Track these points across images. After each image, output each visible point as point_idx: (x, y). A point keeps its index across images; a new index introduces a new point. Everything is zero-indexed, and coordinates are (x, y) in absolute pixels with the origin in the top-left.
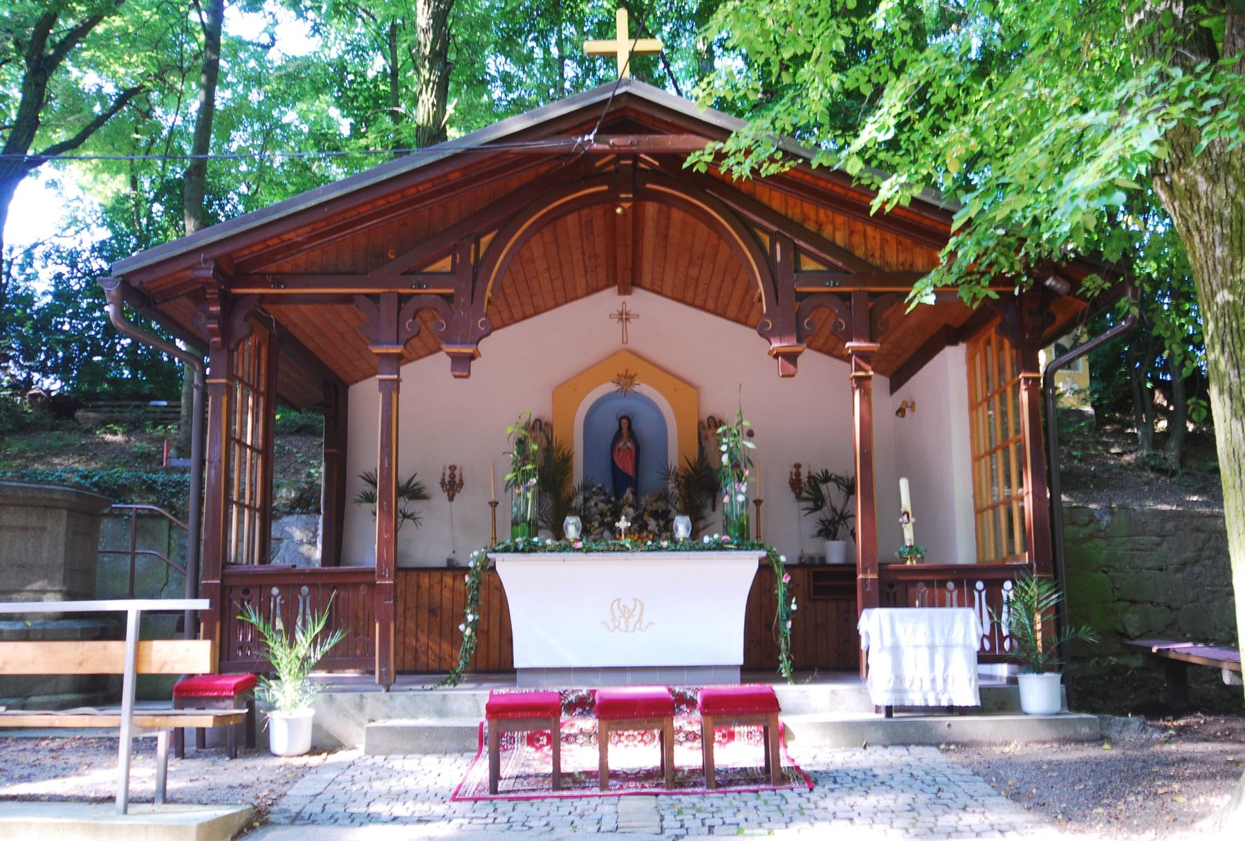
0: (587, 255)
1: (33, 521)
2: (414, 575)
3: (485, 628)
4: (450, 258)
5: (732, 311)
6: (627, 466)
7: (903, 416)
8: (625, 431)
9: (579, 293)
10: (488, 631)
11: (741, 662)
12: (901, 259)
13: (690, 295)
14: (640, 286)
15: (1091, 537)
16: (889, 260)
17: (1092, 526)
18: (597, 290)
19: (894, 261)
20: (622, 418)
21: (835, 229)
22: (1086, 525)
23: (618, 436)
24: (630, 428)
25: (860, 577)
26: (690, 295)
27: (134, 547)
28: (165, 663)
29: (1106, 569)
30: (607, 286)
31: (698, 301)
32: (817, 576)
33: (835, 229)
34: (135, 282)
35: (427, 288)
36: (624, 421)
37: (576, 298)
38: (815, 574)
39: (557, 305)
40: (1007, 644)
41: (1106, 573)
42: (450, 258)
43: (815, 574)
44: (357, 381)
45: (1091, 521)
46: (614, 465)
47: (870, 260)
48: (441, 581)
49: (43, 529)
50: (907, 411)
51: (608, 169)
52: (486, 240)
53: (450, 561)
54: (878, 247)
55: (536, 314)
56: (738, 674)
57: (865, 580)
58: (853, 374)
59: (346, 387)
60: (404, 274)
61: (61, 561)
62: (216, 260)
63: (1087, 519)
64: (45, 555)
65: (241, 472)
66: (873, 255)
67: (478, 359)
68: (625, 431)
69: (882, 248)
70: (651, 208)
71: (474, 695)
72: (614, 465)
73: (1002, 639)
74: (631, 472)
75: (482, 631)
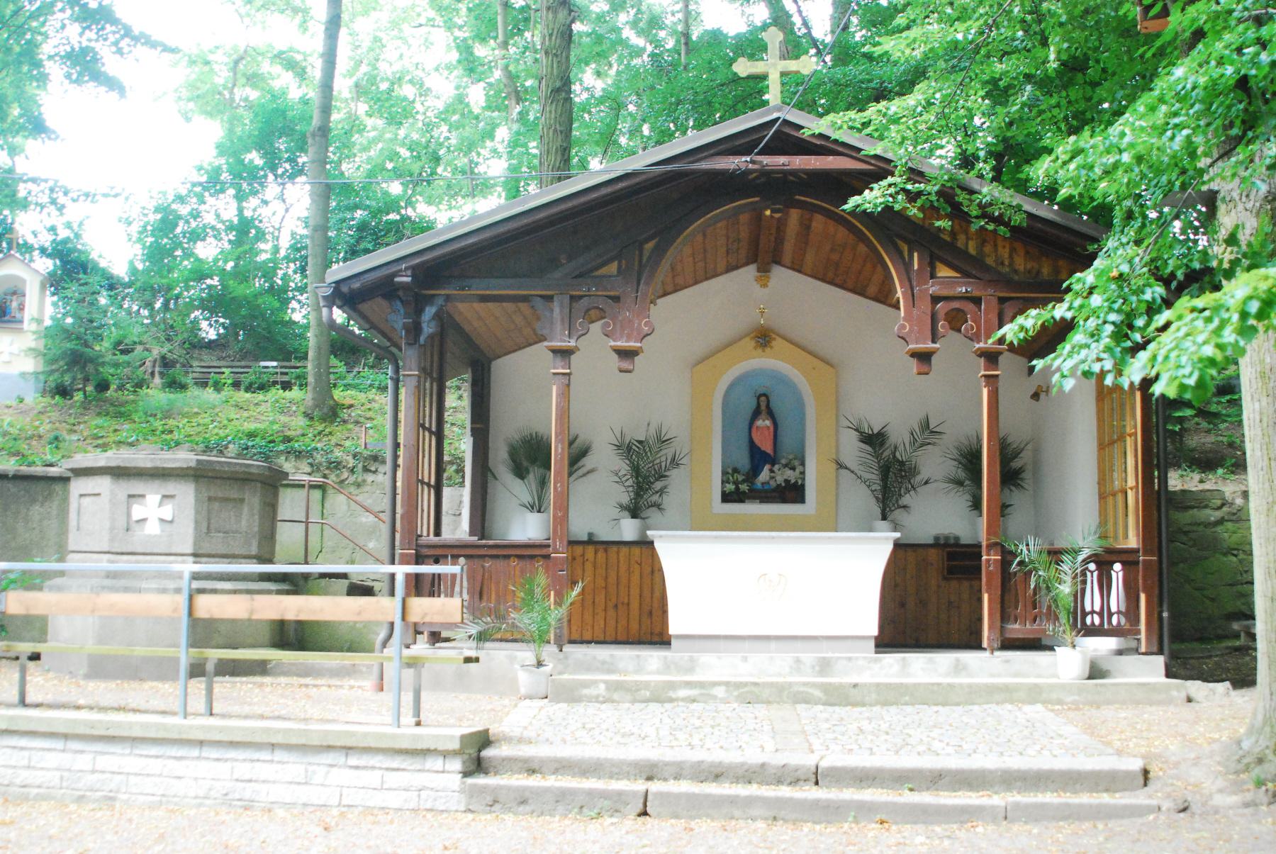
0: (731, 240)
1: (234, 494)
2: (615, 548)
3: (626, 601)
4: (616, 263)
5: (872, 289)
6: (767, 447)
7: (1038, 400)
8: (763, 407)
9: (719, 270)
10: (628, 604)
11: (875, 632)
12: (1029, 266)
13: (830, 275)
14: (779, 263)
15: (1221, 522)
16: (1017, 267)
17: (1225, 509)
18: (737, 267)
19: (1021, 268)
20: (761, 395)
21: (968, 239)
22: (1220, 508)
23: (756, 414)
24: (768, 406)
25: (984, 558)
26: (830, 275)
27: (307, 518)
28: (426, 614)
29: (1235, 552)
30: (747, 264)
31: (838, 280)
32: (951, 556)
33: (968, 239)
34: (345, 289)
35: (597, 290)
36: (763, 399)
37: (716, 275)
38: (949, 553)
39: (696, 282)
40: (1115, 620)
41: (1236, 556)
42: (616, 263)
43: (949, 553)
44: (499, 357)
45: (1223, 505)
46: (751, 442)
47: (1000, 268)
48: (583, 555)
49: (242, 500)
50: (1043, 396)
51: (758, 181)
52: (649, 246)
53: (590, 535)
54: (1006, 255)
55: (676, 291)
56: (872, 644)
57: (988, 561)
58: (983, 373)
59: (490, 361)
60: (576, 277)
61: (256, 529)
62: (414, 268)
63: (1219, 502)
64: (244, 523)
65: (424, 457)
66: (1002, 263)
67: (641, 354)
68: (763, 407)
69: (1011, 257)
70: (795, 215)
71: (638, 656)
72: (751, 442)
73: (1110, 615)
74: (769, 450)
75: (623, 604)
